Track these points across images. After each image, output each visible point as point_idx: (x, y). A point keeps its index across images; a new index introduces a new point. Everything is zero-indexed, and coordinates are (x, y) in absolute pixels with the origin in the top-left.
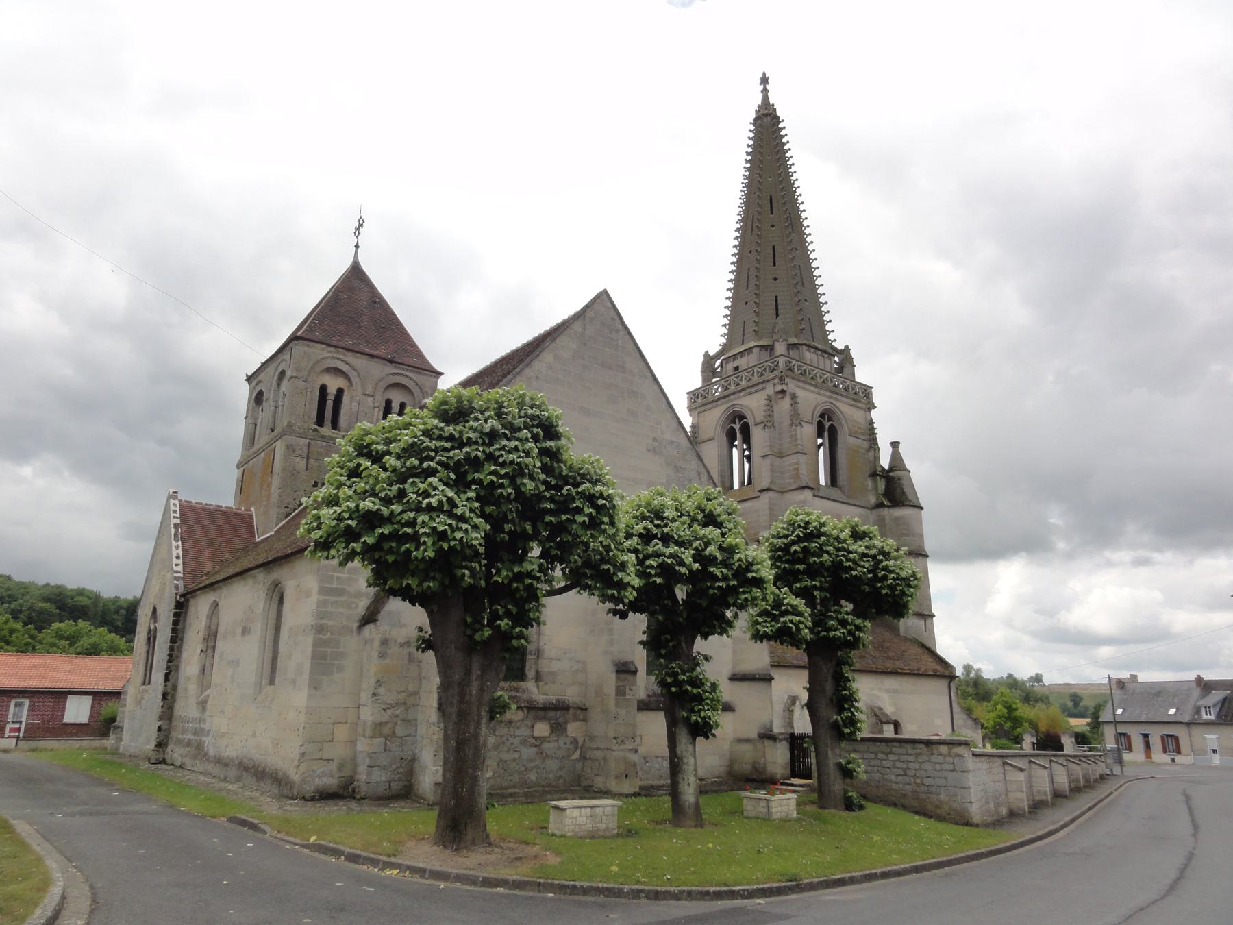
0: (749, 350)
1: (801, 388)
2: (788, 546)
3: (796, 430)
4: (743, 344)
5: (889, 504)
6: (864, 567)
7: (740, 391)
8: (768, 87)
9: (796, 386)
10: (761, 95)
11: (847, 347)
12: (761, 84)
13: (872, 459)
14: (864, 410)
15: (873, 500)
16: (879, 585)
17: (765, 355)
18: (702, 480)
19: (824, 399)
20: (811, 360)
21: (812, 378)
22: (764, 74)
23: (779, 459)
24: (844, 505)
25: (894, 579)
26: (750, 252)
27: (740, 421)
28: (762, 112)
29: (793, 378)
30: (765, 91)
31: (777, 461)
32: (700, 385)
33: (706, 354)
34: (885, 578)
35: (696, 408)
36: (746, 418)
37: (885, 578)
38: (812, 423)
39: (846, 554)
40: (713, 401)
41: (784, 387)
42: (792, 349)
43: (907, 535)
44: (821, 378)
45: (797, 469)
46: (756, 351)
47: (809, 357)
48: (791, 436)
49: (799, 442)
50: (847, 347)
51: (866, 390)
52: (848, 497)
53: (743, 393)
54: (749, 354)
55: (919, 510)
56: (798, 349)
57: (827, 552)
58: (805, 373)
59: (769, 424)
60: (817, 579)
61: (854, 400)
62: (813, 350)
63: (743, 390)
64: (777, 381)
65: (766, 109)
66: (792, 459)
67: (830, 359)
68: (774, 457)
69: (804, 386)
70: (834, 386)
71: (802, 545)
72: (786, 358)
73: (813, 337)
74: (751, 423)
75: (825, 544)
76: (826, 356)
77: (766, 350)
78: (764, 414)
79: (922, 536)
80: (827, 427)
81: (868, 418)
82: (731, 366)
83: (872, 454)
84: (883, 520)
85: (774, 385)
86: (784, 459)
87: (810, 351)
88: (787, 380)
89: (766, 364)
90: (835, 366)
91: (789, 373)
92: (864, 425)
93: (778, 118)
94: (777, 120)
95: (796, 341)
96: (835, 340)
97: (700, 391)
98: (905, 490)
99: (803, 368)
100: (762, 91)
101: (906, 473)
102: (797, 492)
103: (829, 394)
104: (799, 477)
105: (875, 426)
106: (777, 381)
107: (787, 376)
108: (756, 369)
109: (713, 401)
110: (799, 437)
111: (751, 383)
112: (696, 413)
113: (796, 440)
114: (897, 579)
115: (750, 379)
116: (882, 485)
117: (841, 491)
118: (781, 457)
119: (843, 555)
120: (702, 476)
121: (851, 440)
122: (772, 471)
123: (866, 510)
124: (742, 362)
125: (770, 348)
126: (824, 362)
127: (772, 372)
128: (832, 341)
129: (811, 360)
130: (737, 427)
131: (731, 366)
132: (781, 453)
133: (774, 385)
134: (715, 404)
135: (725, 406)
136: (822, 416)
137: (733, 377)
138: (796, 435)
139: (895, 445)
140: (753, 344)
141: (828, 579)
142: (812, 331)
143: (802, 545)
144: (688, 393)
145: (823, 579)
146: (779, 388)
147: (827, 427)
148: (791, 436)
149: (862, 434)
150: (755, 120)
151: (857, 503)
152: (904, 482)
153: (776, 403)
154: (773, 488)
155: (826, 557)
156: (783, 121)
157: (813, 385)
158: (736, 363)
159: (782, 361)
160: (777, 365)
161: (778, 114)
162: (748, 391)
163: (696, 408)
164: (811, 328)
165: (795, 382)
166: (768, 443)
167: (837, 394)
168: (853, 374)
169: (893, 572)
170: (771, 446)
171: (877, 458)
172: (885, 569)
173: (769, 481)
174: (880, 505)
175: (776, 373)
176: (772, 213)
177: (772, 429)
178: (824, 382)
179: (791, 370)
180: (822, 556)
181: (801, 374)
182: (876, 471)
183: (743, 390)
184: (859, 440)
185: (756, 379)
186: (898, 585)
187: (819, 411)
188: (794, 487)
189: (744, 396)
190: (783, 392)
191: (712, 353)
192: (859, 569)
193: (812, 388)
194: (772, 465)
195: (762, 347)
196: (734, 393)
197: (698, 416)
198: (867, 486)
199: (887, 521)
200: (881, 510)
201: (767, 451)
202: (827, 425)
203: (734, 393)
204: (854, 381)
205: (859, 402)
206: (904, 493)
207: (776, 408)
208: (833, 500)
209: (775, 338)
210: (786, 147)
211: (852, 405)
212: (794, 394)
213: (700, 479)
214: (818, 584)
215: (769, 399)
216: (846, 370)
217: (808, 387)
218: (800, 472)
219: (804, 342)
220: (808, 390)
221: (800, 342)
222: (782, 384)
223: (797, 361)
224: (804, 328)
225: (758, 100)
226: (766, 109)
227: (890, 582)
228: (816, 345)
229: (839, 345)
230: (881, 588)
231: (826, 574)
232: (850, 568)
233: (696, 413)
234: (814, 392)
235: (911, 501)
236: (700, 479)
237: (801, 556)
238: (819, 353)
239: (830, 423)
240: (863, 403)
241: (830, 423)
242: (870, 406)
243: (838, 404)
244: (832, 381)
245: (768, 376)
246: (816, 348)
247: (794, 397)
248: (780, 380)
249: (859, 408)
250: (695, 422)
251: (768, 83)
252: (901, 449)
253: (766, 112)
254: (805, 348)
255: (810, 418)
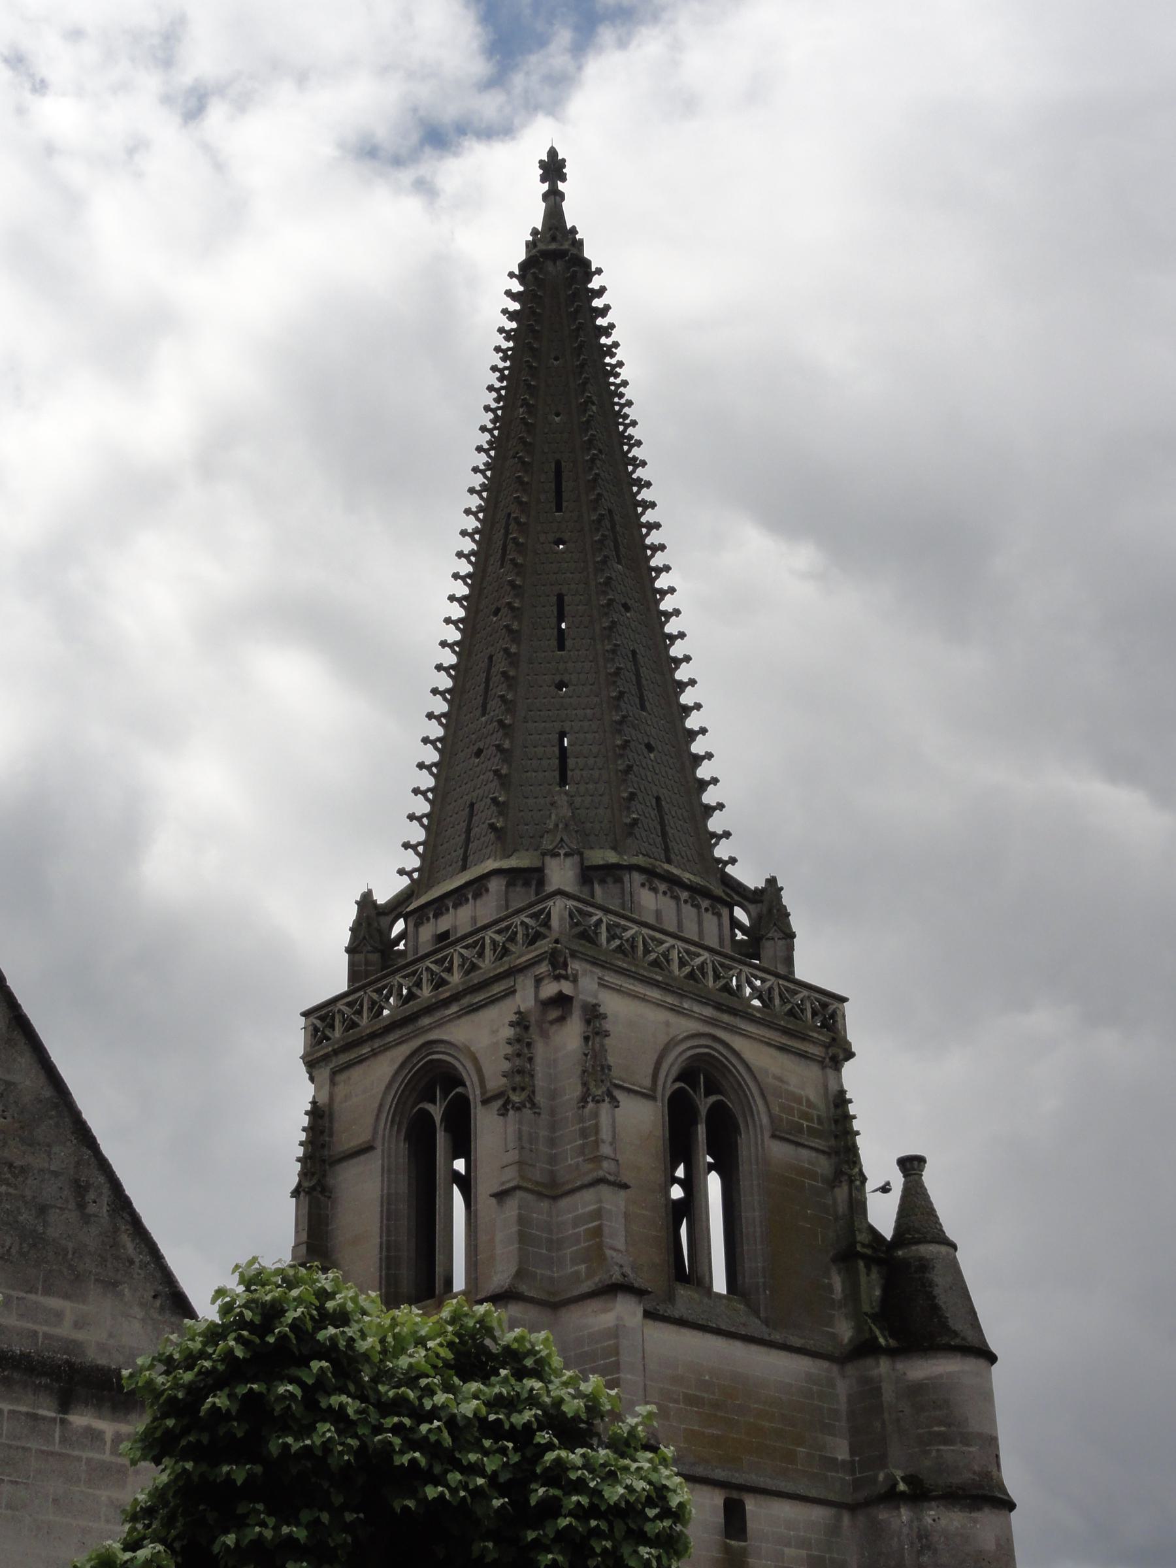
0: (478, 886)
1: (619, 991)
2: (197, 1393)
3: (596, 1115)
4: (464, 868)
5: (893, 1343)
6: (476, 1469)
7: (446, 1003)
8: (561, 186)
9: (603, 985)
10: (541, 207)
11: (772, 881)
12: (543, 180)
13: (842, 1208)
14: (822, 1063)
15: (845, 1331)
16: (531, 1535)
17: (521, 897)
18: (91, 1209)
19: (693, 1026)
20: (658, 913)
21: (656, 963)
22: (553, 153)
23: (545, 1205)
24: (754, 1349)
25: (581, 1513)
26: (479, 753)
27: (445, 1094)
28: (541, 246)
29: (594, 963)
30: (554, 199)
31: (541, 1210)
32: (344, 988)
33: (366, 902)
34: (551, 1508)
35: (326, 1058)
36: (464, 1085)
37: (551, 1508)
38: (650, 1096)
39: (407, 1421)
40: (373, 1036)
41: (567, 988)
42: (603, 882)
43: (946, 1439)
44: (682, 963)
45: (598, 1232)
46: (496, 886)
47: (653, 907)
48: (584, 1133)
49: (606, 1150)
50: (772, 881)
51: (825, 1006)
52: (766, 1322)
53: (454, 1008)
54: (477, 896)
55: (981, 1363)
56: (619, 880)
57: (339, 1417)
58: (634, 947)
59: (515, 1098)
60: (306, 1516)
61: (786, 1032)
62: (662, 887)
63: (455, 998)
64: (544, 968)
65: (554, 239)
66: (585, 1202)
67: (719, 915)
68: (530, 1197)
69: (629, 985)
70: (727, 988)
71: (241, 1390)
72: (571, 903)
73: (667, 850)
74: (474, 1093)
75: (321, 1386)
76: (705, 903)
77: (527, 884)
78: (506, 1066)
79: (993, 1441)
80: (703, 1111)
81: (833, 1087)
82: (427, 933)
83: (842, 1193)
84: (876, 1392)
85: (538, 981)
86: (564, 1203)
87: (654, 890)
88: (575, 966)
89: (516, 920)
90: (740, 936)
91: (578, 946)
92: (821, 1107)
93: (588, 263)
94: (585, 270)
95: (612, 858)
96: (733, 861)
97: (340, 1005)
98: (942, 1300)
99: (628, 934)
100: (545, 197)
101: (944, 1249)
102: (594, 1305)
103: (708, 1012)
104: (602, 1258)
105: (852, 1109)
106: (544, 968)
107: (574, 954)
108: (489, 935)
109: (373, 1036)
110: (605, 1134)
111: (476, 977)
112: (324, 1073)
113: (597, 1144)
114: (593, 1511)
115: (474, 967)
116: (872, 1287)
117: (748, 1304)
118: (555, 1198)
119: (397, 1429)
120: (91, 1196)
121: (779, 1151)
122: (524, 1238)
123: (825, 1364)
124: (460, 919)
125: (532, 877)
126: (700, 923)
127: (532, 942)
128: (726, 863)
129: (658, 913)
130: (437, 1111)
131: (427, 933)
132: (553, 1182)
133: (538, 981)
134: (377, 1043)
135: (405, 1050)
136: (688, 1075)
137: (428, 963)
138: (597, 1128)
139: (911, 1166)
140: (491, 865)
141: (349, 1517)
142: (664, 834)
143: (241, 1390)
144: (305, 1014)
145: (325, 1517)
146: (550, 989)
147: (703, 1111)
148: (584, 1133)
149: (812, 1132)
150: (523, 266)
151: (797, 1342)
152: (940, 1279)
153: (544, 1035)
154: (524, 1288)
155: (326, 1430)
156: (599, 271)
157: (656, 984)
158: (444, 924)
159: (558, 909)
160: (546, 924)
161: (587, 254)
162: (465, 1001)
163: (326, 1058)
164: (662, 824)
165: (598, 972)
166: (513, 1156)
167: (733, 1012)
168: (789, 961)
169: (579, 1486)
170: (520, 1163)
171: (858, 1206)
172: (557, 1475)
173: (513, 1270)
174: (864, 1349)
175: (544, 946)
176: (559, 508)
177: (527, 1112)
178: (691, 976)
179: (587, 936)
180: (310, 1430)
181: (620, 949)
182: (853, 1244)
183: (455, 998)
184: (805, 1153)
185: (488, 965)
186: (597, 1533)
187: (673, 1064)
188: (586, 1287)
189: (459, 1016)
190: (562, 1001)
191: (382, 897)
192: (455, 1477)
193: (655, 994)
194: (522, 1220)
195: (513, 876)
196: (429, 1010)
197: (333, 1083)
198: (830, 1288)
199: (888, 1394)
200: (869, 1362)
201: (510, 1177)
202: (704, 1104)
203: (429, 1010)
204: (789, 977)
205: (804, 1038)
206: (935, 1309)
207: (540, 1051)
208: (718, 1332)
209: (547, 844)
210: (597, 303)
211: (782, 1049)
212: (595, 1006)
213: (81, 1206)
214: (300, 1534)
215: (521, 1022)
216: (769, 949)
217: (640, 988)
218: (607, 1241)
219: (640, 860)
220: (644, 999)
221: (626, 860)
222: (558, 978)
223: (607, 911)
224: (635, 822)
225: (536, 217)
226: (554, 239)
227: (563, 1522)
228: (676, 871)
229: (749, 875)
230: (539, 1546)
231: (338, 1500)
232: (416, 1476)
233: (324, 1073)
234: (659, 1005)
235: (956, 1334)
236: (81, 1206)
237: (239, 1429)
238: (684, 895)
239: (713, 1099)
240: (814, 1042)
241: (713, 1099)
242: (840, 1053)
243: (737, 1043)
244: (717, 977)
245: (521, 954)
246: (674, 882)
247: (593, 1015)
248: (554, 965)
249: (803, 1056)
250: (323, 1099)
251: (563, 178)
252: (930, 1178)
253: (553, 246)
254: (637, 878)
255: (647, 1082)
